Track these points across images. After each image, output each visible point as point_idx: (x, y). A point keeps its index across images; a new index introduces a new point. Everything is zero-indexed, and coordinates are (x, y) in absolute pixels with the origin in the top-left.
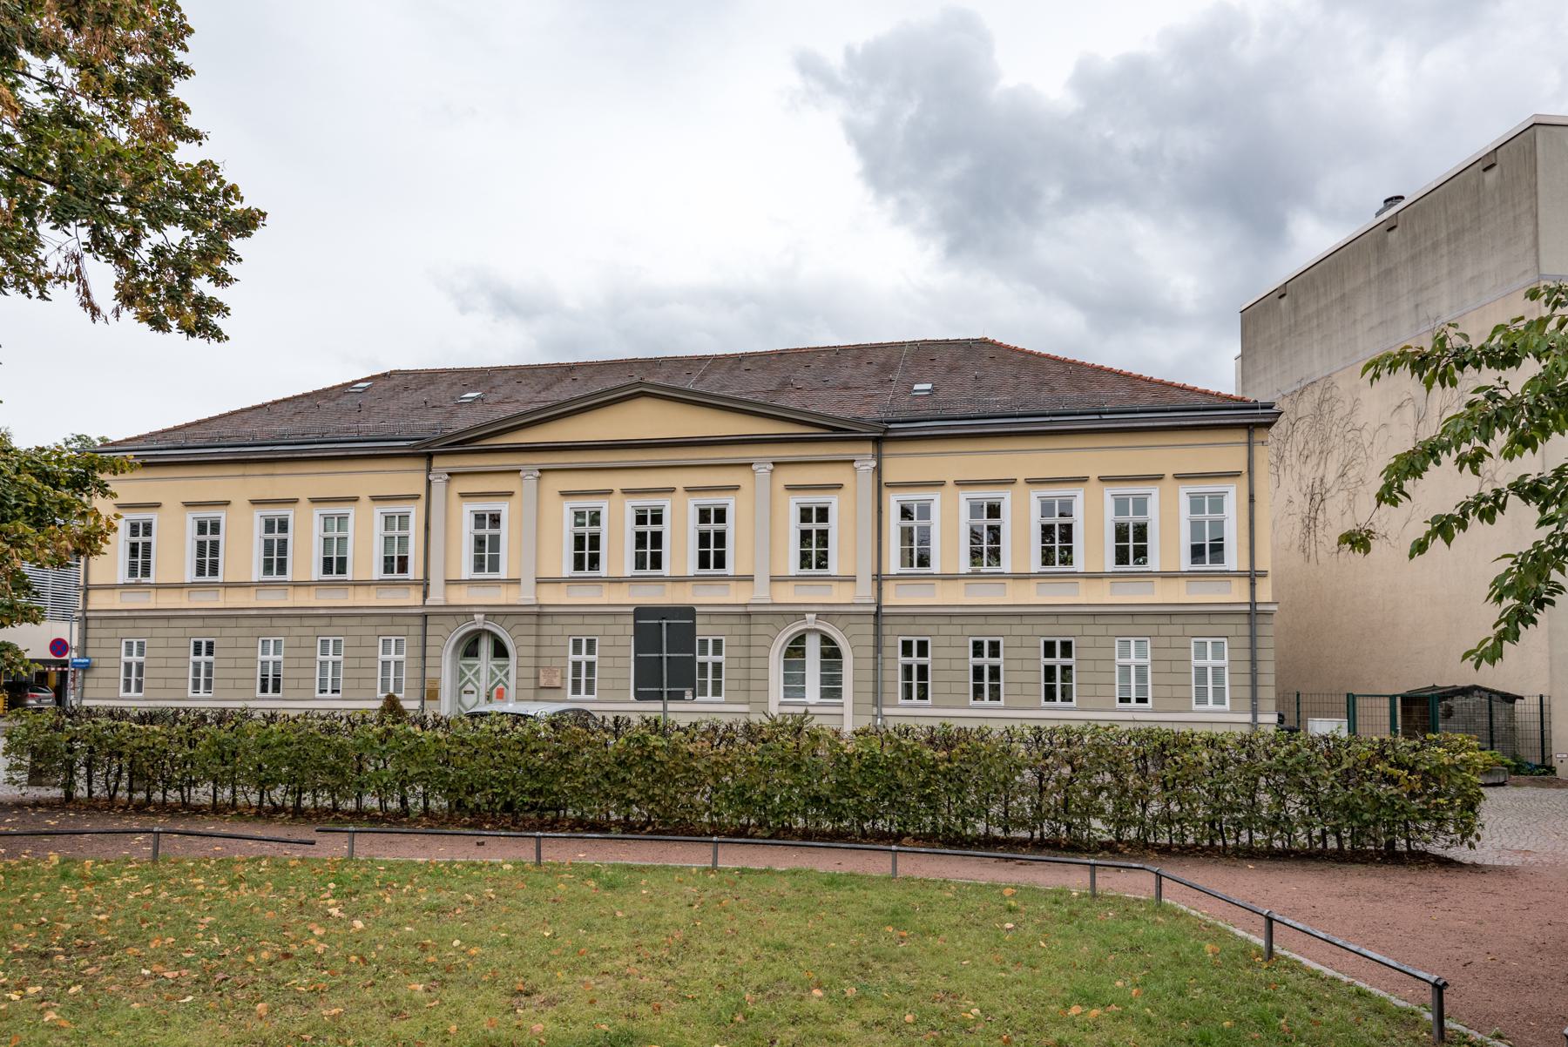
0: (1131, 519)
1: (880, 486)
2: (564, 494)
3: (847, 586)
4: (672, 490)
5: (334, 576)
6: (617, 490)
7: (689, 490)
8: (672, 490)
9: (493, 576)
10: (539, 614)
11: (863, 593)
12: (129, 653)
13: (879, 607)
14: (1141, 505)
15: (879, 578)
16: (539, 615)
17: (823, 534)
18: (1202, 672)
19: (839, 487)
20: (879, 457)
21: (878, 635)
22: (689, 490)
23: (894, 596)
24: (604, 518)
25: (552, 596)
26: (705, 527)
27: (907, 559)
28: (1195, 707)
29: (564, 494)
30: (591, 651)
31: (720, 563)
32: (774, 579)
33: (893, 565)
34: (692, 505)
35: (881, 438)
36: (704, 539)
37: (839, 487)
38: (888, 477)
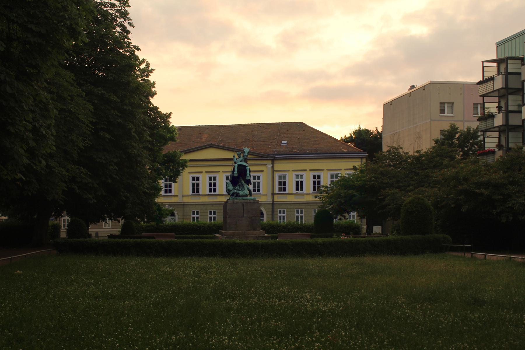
0: (299, 180)
1: (273, 171)
2: (190, 173)
3: (265, 197)
4: (219, 172)
5: (213, 193)
6: (204, 172)
7: (223, 172)
8: (219, 172)
9: (198, 194)
10: (184, 205)
11: (269, 198)
12: (194, 214)
13: (273, 202)
14: (302, 176)
15: (273, 194)
16: (183, 205)
17: (259, 183)
18: (280, 217)
19: (263, 171)
20: (273, 164)
21: (273, 209)
22: (223, 172)
23: (277, 199)
24: (217, 178)
25: (186, 200)
26: (211, 182)
27: (280, 190)
28: (104, 227)
29: (190, 173)
30: (197, 214)
31: (198, 191)
32: (183, 196)
33: (277, 191)
34: (207, 176)
35: (273, 159)
36: (194, 185)
37: (263, 171)
38: (275, 169)
